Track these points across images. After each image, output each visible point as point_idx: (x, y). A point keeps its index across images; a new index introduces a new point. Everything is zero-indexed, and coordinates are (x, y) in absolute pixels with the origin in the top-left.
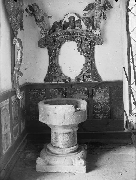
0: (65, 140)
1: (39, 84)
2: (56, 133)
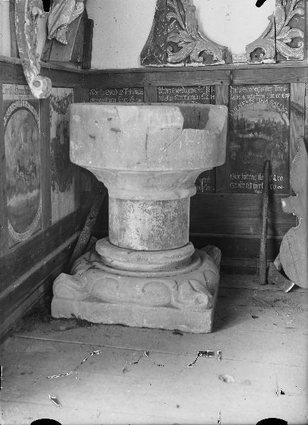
0: (148, 227)
1: (101, 71)
2: (120, 201)
